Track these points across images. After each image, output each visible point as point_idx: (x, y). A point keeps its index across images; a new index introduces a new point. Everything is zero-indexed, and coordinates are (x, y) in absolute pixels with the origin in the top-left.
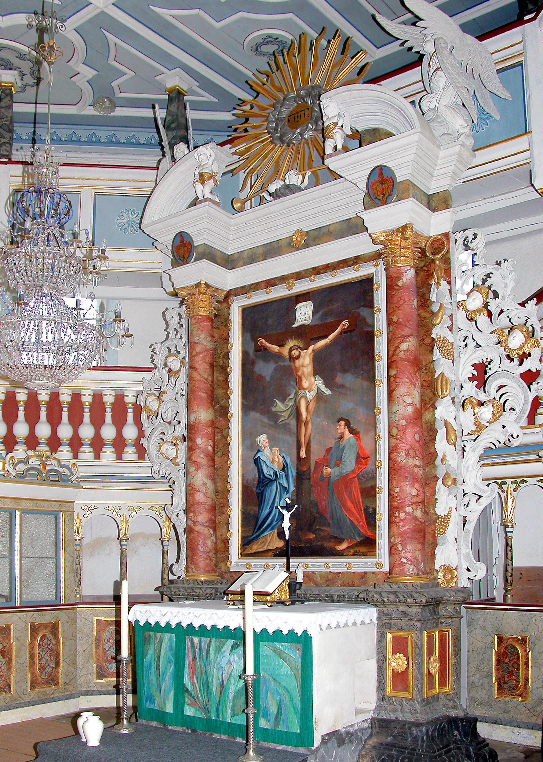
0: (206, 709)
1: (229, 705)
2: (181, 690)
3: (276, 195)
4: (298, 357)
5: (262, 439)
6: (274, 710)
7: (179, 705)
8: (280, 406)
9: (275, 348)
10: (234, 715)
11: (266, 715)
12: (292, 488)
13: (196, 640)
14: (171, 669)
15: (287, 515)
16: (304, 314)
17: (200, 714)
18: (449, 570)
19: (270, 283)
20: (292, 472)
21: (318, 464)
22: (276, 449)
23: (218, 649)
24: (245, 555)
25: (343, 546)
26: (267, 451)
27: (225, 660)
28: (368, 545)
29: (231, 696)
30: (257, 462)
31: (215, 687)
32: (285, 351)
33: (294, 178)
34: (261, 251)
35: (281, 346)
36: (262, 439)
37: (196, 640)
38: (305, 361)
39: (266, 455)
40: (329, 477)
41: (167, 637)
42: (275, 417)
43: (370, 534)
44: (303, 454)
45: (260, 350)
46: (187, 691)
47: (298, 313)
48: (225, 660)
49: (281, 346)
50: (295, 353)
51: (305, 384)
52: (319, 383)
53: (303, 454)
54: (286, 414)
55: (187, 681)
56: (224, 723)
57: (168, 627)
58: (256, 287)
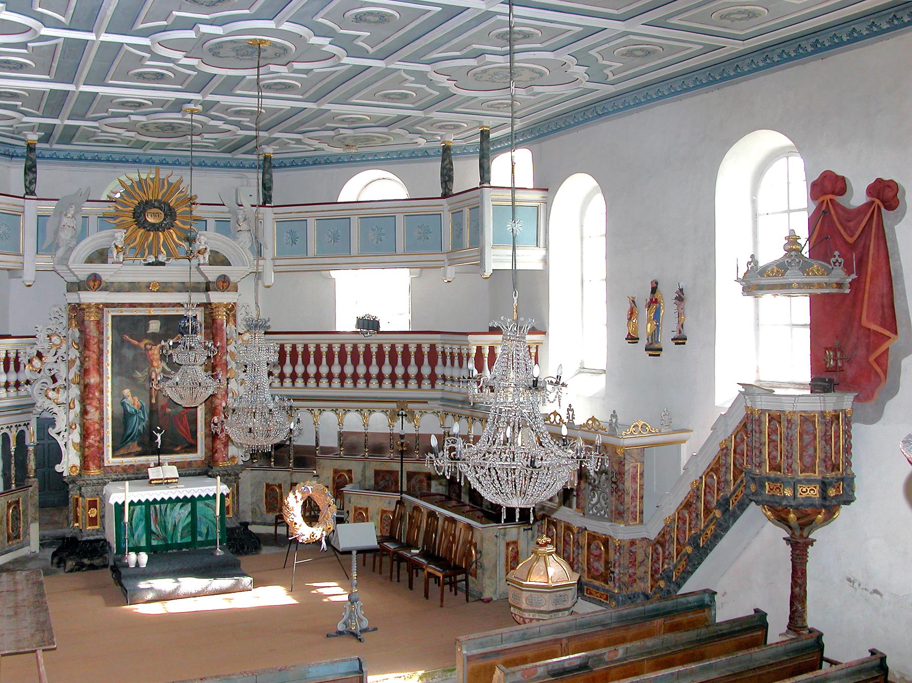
0: (165, 539)
1: (179, 535)
2: (149, 533)
3: (149, 264)
4: (151, 349)
5: (127, 392)
6: (204, 531)
7: (148, 541)
8: (138, 374)
9: (136, 343)
10: (182, 538)
11: (201, 535)
12: (147, 419)
13: (158, 506)
14: (142, 525)
15: (159, 436)
16: (155, 327)
17: (161, 543)
18: (233, 457)
19: (132, 305)
20: (147, 411)
21: (163, 407)
22: (136, 398)
23: (172, 509)
24: (113, 456)
25: (179, 448)
26: (130, 398)
27: (176, 513)
28: (192, 448)
29: (180, 530)
30: (123, 404)
31: (170, 527)
32: (142, 345)
33: (162, 258)
34: (127, 286)
35: (139, 341)
36: (127, 392)
37: (158, 506)
38: (155, 352)
39: (129, 400)
40: (169, 414)
41: (138, 508)
42: (134, 380)
43: (193, 442)
44: (154, 401)
45: (123, 341)
46: (154, 533)
47: (151, 325)
48: (176, 513)
49: (139, 341)
50: (149, 347)
51: (155, 364)
52: (164, 364)
53: (154, 401)
54: (143, 380)
55: (153, 528)
56: (177, 543)
57: (140, 502)
58: (122, 305)
